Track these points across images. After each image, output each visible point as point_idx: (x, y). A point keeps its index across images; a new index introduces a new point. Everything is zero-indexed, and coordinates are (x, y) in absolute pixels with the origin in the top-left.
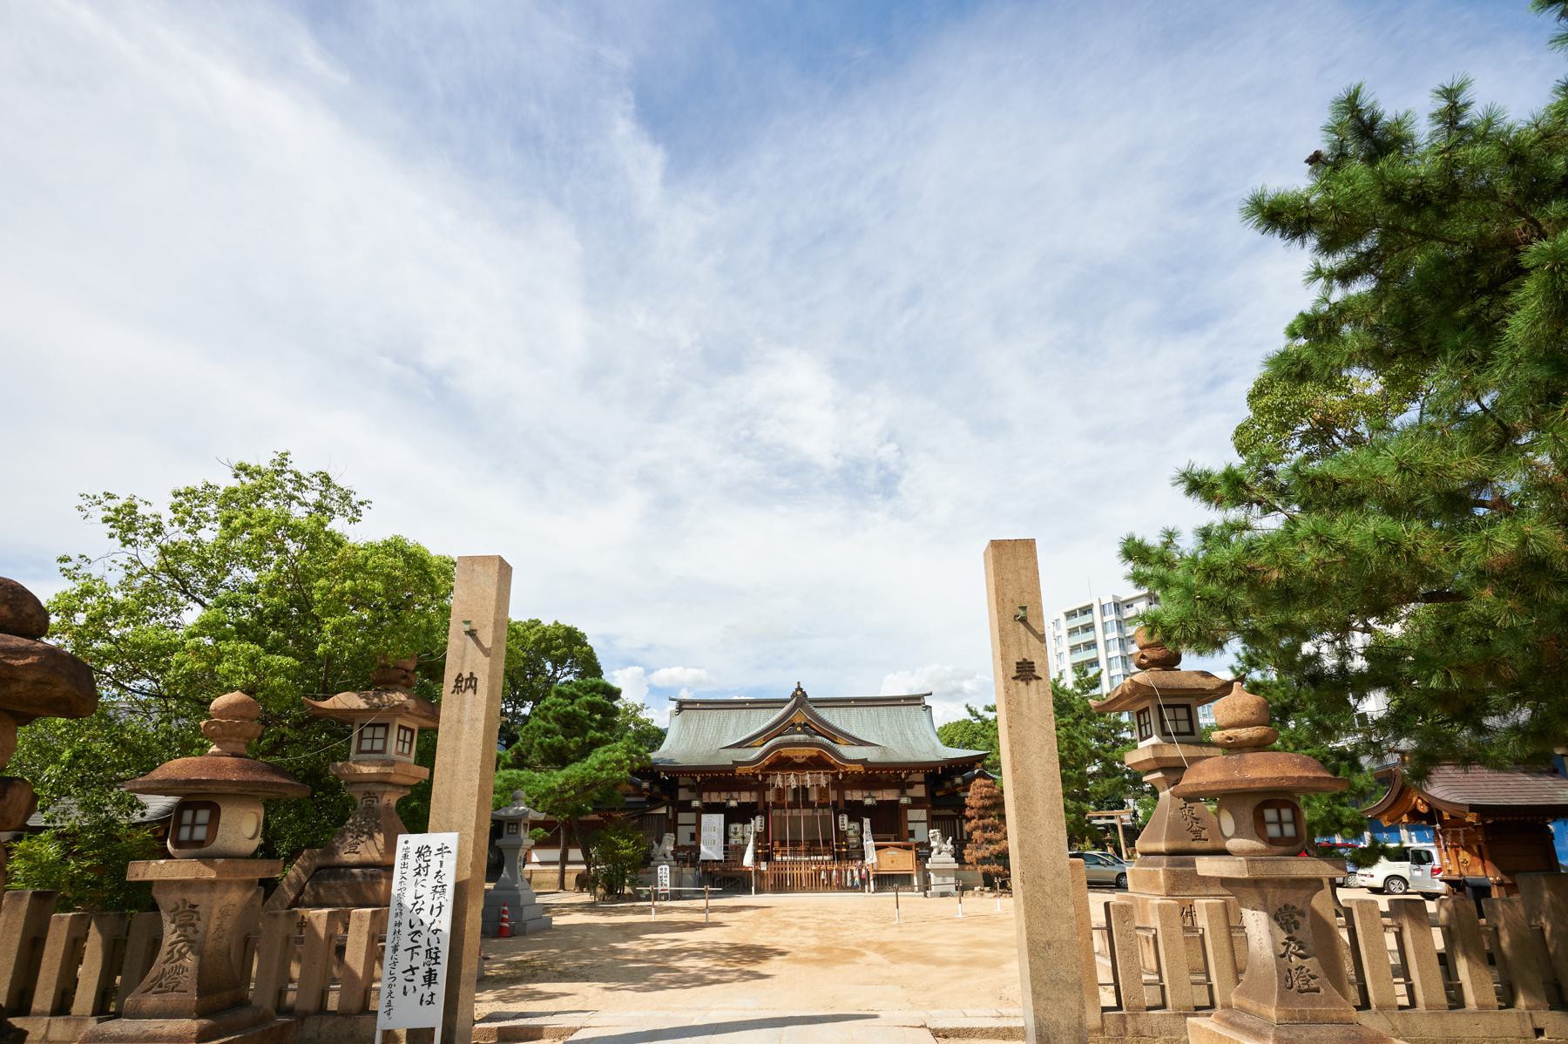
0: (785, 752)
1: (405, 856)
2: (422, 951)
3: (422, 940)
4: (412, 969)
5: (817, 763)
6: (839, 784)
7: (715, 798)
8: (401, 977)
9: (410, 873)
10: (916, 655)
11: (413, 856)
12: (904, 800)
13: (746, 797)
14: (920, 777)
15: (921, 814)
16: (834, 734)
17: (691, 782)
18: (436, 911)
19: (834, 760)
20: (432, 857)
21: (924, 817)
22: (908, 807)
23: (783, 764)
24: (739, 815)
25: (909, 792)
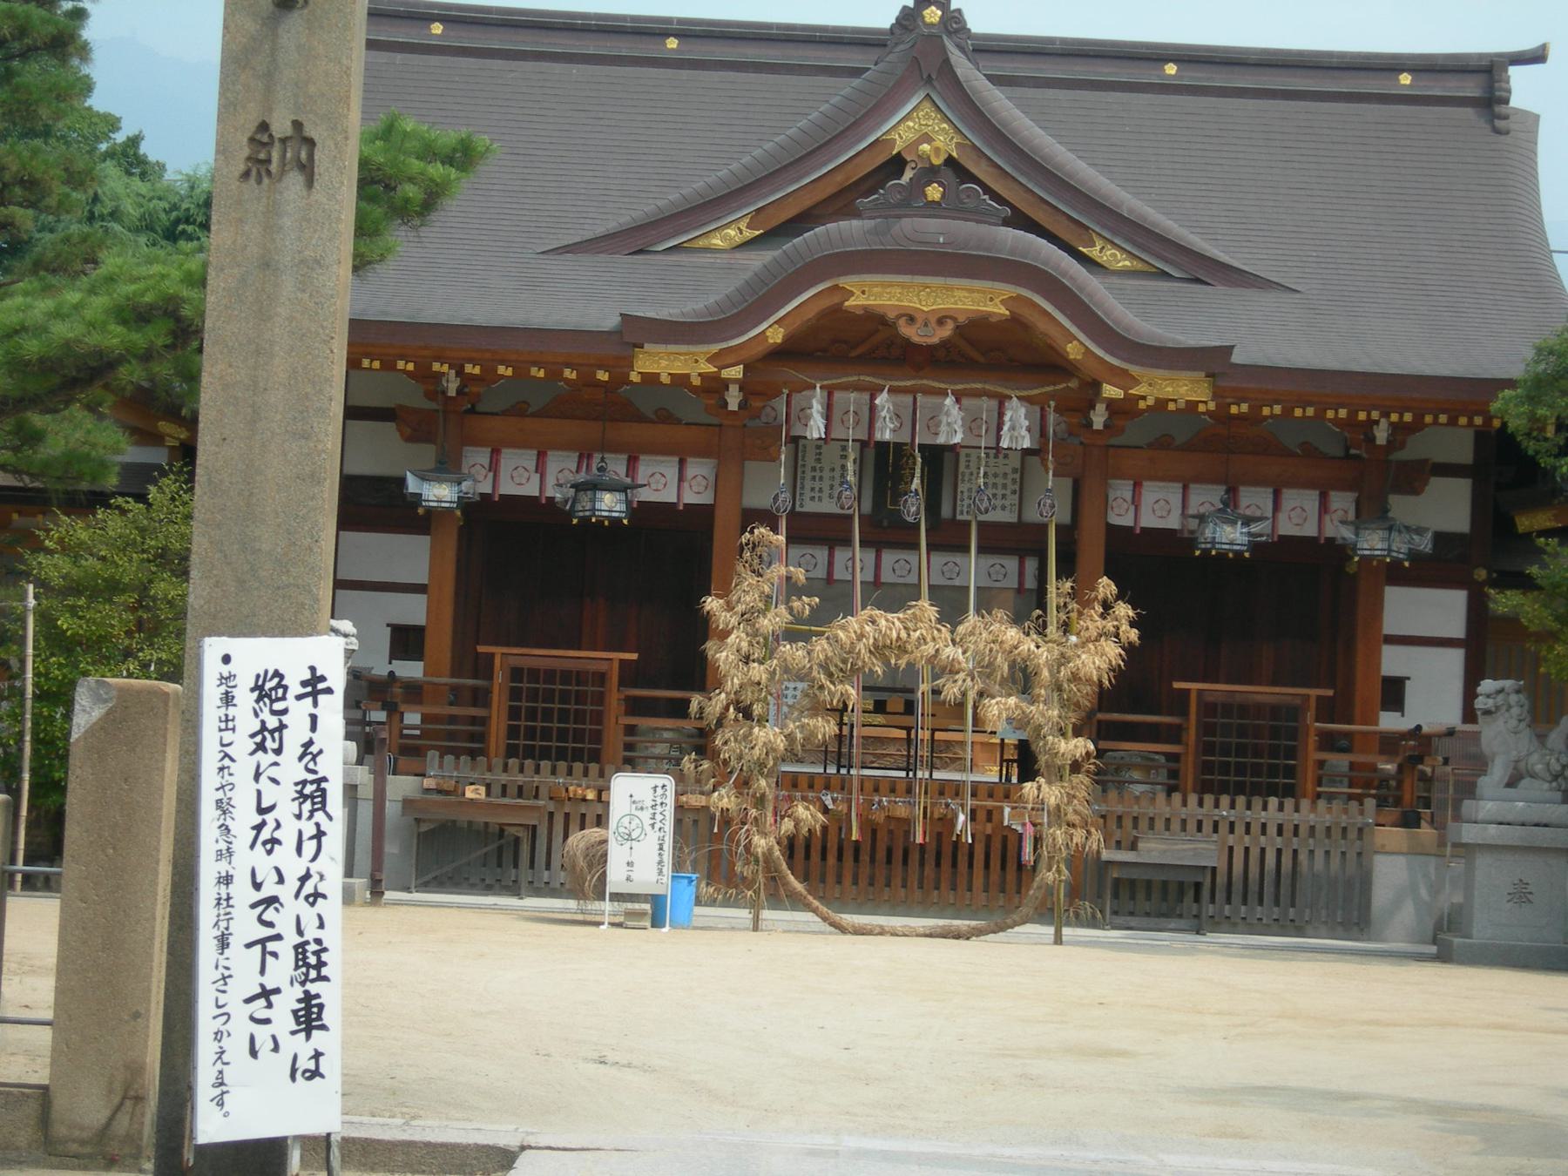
0: (870, 293)
1: (228, 699)
2: (285, 949)
3: (283, 921)
4: (266, 994)
8: (240, 1012)
9: (242, 744)
11: (245, 698)
12: (1372, 543)
14: (1458, 446)
15: (1445, 611)
16: (1061, 211)
17: (413, 397)
18: (309, 847)
19: (1077, 346)
20: (291, 702)
21: (1456, 627)
22: (1398, 574)
25: (1401, 506)
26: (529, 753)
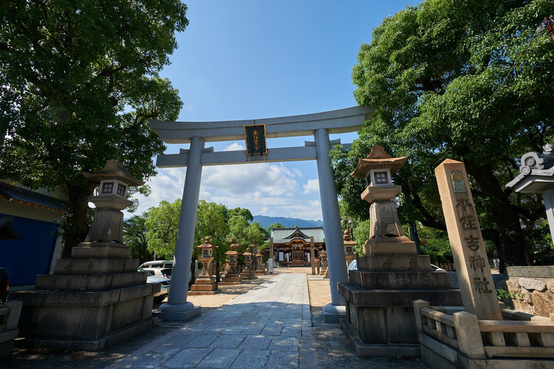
5: (301, 243)
6: (305, 246)
7: (281, 249)
10: (315, 150)
13: (287, 249)
16: (304, 237)
23: (294, 243)
24: (285, 253)
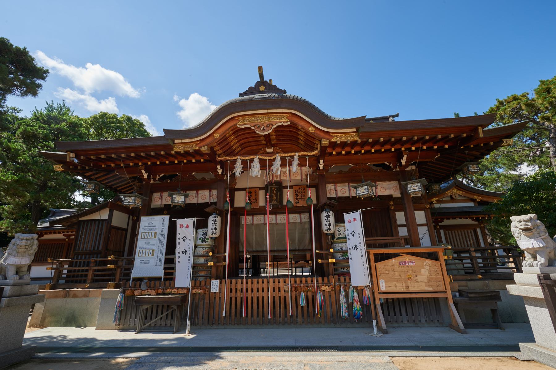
23: (251, 143)
26: (72, 281)
